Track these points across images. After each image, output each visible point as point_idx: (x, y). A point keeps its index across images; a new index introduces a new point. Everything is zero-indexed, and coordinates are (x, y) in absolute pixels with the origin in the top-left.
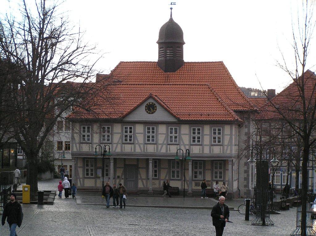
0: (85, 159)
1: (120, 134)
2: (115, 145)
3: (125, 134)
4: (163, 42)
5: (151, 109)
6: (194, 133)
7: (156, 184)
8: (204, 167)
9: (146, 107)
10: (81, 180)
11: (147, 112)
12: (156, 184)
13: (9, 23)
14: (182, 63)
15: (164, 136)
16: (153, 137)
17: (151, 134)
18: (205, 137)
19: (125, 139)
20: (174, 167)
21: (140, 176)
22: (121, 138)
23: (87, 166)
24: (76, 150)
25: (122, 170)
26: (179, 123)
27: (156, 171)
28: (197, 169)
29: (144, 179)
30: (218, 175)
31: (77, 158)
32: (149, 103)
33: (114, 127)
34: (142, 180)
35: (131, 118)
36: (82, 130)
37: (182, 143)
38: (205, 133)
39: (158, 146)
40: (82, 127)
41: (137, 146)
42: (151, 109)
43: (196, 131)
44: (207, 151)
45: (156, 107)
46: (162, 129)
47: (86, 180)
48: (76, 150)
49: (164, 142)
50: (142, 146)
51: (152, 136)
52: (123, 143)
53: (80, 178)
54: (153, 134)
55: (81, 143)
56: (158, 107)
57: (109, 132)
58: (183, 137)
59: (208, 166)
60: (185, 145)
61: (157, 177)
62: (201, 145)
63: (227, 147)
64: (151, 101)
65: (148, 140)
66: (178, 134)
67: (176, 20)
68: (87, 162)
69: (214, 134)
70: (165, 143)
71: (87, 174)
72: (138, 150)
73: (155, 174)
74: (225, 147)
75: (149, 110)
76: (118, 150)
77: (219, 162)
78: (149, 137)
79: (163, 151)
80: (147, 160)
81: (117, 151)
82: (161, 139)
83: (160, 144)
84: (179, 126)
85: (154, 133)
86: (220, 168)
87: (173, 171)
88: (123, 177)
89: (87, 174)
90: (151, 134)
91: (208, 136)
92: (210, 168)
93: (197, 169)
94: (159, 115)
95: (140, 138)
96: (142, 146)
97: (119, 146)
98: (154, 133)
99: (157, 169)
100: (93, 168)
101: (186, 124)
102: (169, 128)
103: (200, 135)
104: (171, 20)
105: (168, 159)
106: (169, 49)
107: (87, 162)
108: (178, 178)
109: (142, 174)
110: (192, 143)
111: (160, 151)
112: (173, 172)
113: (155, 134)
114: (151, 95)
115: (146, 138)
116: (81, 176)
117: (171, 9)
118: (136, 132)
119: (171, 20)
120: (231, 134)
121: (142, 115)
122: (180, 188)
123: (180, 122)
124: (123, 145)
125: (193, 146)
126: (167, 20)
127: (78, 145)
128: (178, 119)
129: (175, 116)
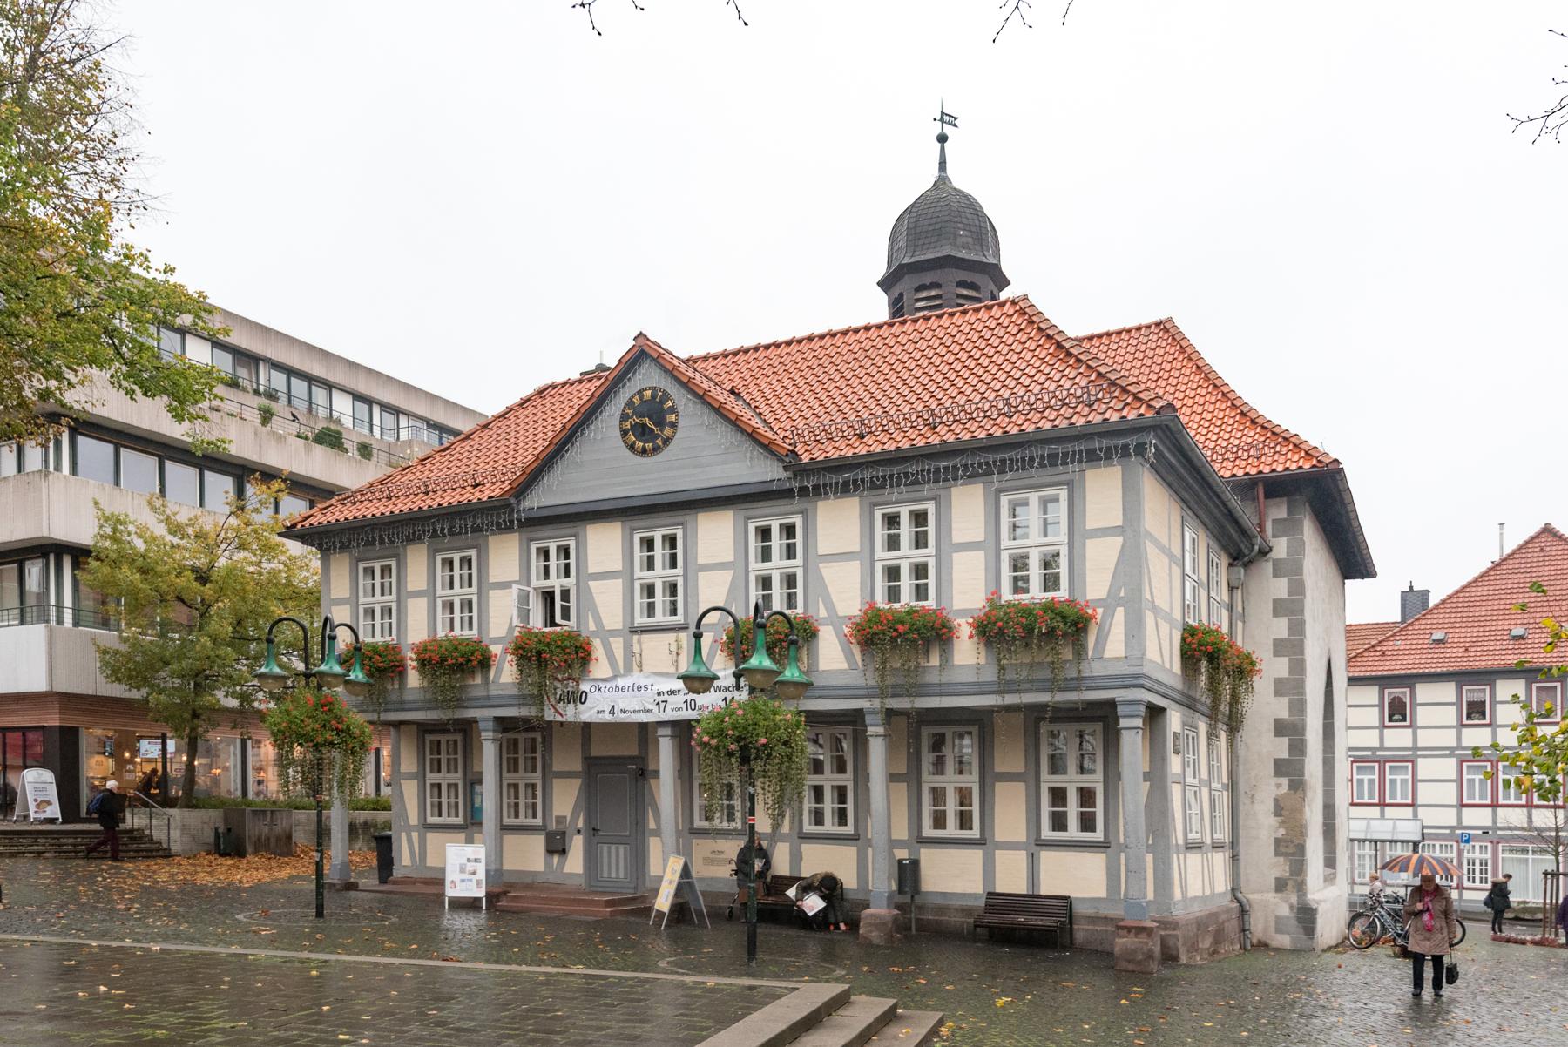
0: (926, 733)
1: (1120, 539)
3: (883, 556)
8: (546, 767)
10: (415, 835)
11: (632, 447)
15: (727, 576)
17: (906, 556)
18: (494, 594)
19: (1016, 579)
20: (1057, 766)
23: (1057, 766)
25: (575, 785)
26: (803, 492)
28: (822, 772)
32: (640, 393)
33: (333, 567)
36: (880, 533)
38: (957, 538)
42: (649, 428)
45: (673, 410)
53: (409, 829)
54: (891, 557)
55: (634, 631)
58: (828, 571)
59: (568, 759)
64: (647, 379)
66: (799, 561)
67: (960, 179)
68: (938, 743)
71: (1059, 823)
73: (1065, 805)
75: (642, 432)
84: (396, 556)
87: (933, 790)
88: (580, 825)
89: (1059, 823)
92: (1019, 766)
93: (822, 772)
100: (972, 780)
101: (845, 489)
102: (878, 514)
108: (966, 834)
112: (1059, 796)
113: (931, 549)
116: (413, 818)
118: (700, 561)
120: (1130, 527)
121: (605, 467)
125: (645, 637)
126: (924, 181)
128: (789, 459)
129: (768, 448)
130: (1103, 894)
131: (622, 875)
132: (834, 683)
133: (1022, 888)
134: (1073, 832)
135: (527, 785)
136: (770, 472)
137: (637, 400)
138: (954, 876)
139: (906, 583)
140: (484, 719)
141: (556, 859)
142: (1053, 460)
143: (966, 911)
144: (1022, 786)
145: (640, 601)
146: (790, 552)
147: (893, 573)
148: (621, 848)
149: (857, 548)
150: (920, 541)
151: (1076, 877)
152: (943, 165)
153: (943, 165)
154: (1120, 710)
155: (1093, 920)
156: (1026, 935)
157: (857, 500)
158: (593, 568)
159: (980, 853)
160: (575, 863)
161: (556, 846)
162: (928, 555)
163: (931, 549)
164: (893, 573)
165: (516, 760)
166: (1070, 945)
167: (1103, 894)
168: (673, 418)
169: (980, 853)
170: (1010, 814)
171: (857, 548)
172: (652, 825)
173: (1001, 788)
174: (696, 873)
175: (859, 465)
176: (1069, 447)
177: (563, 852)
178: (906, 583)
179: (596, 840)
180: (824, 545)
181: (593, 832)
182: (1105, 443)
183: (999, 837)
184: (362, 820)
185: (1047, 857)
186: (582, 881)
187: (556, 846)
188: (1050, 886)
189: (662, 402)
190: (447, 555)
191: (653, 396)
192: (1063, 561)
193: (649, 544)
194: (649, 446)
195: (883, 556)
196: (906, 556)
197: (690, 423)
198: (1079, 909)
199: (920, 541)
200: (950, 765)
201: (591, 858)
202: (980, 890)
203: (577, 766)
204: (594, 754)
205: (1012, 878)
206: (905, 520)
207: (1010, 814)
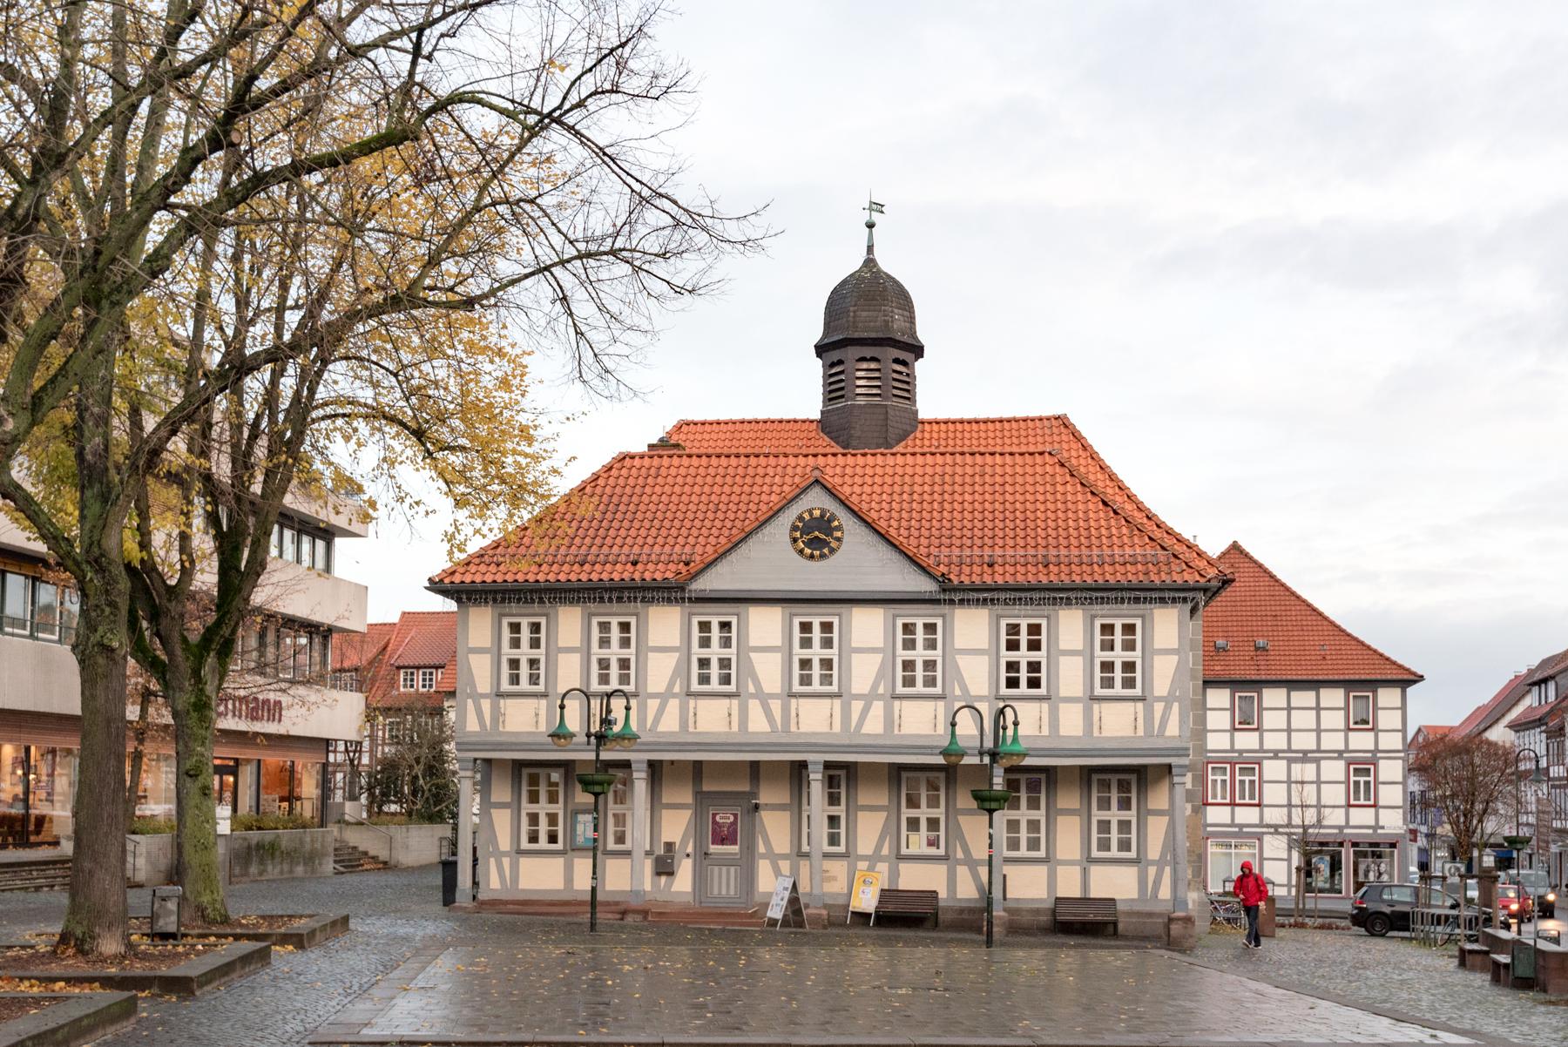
0: (525, 772)
2: (653, 705)
3: (698, 652)
4: (131, 294)
5: (816, 538)
6: (910, 645)
7: (834, 879)
9: (794, 528)
10: (506, 861)
12: (834, 879)
13: (595, 93)
14: (914, 422)
15: (878, 658)
16: (827, 664)
18: (1064, 661)
21: (767, 843)
22: (682, 670)
23: (913, 803)
24: (477, 729)
25: (687, 815)
27: (833, 820)
29: (784, 857)
30: (1114, 836)
31: (488, 761)
34: (774, 858)
35: (709, 583)
36: (596, 634)
37: (752, 689)
38: (1063, 646)
39: (1057, 709)
40: (505, 622)
41: (754, 707)
42: (816, 538)
43: (920, 636)
44: (1071, 723)
45: (839, 528)
46: (765, 627)
47: (524, 862)
48: (477, 729)
49: (875, 686)
50: (776, 706)
51: (1029, 664)
52: (689, 694)
53: (499, 855)
54: (806, 653)
56: (853, 535)
57: (1129, 646)
60: (764, 698)
61: (842, 849)
62: (1142, 699)
63: (1168, 708)
64: (816, 501)
65: (704, 679)
68: (534, 781)
69: (802, 647)
70: (881, 690)
71: (534, 838)
72: (758, 724)
74: (1159, 708)
75: (815, 543)
76: (669, 724)
77: (1114, 778)
78: (805, 664)
79: (874, 725)
80: (803, 765)
81: (661, 728)
82: (863, 673)
83: (1160, 699)
84: (546, 615)
85: (1133, 649)
86: (1125, 804)
88: (690, 849)
90: (715, 652)
91: (1079, 660)
94: (860, 562)
95: (769, 671)
96: (776, 706)
97: (673, 705)
98: (1133, 649)
99: (839, 811)
100: (558, 809)
102: (595, 621)
103: (1007, 656)
104: (870, 262)
105: (1082, 767)
106: (865, 365)
107: (534, 781)
108: (553, 846)
109: (775, 828)
110: (900, 689)
111: (657, 720)
112: (534, 819)
113: (543, 650)
114: (817, 473)
115: (1098, 674)
116: (505, 843)
117: (871, 226)
119: (870, 262)
121: (771, 560)
122: (943, 894)
123: (952, 593)
124: (692, 702)
125: (801, 701)
126: (853, 262)
127: (486, 705)
130: (1135, 896)
131: (732, 892)
132: (473, 739)
133: (1077, 894)
134: (1114, 852)
135: (1120, 822)
136: (925, 586)
137: (807, 517)
138: (1028, 886)
139: (614, 671)
140: (815, 763)
141: (663, 879)
142: (1137, 600)
143: (1037, 911)
144: (1077, 819)
145: (505, 671)
146: (726, 643)
147: (604, 664)
148: (732, 869)
149: (779, 643)
150: (625, 643)
151: (1116, 884)
152: (870, 249)
153: (870, 249)
154: (634, 766)
155: (1130, 914)
156: (1081, 924)
157: (678, 609)
158: (754, 641)
159: (945, 867)
160: (683, 881)
161: (664, 867)
162: (540, 653)
163: (543, 650)
164: (514, 664)
165: (1129, 799)
166: (1115, 934)
167: (1135, 896)
168: (838, 534)
169: (945, 867)
170: (1069, 837)
171: (779, 643)
172: (762, 849)
173: (666, 815)
174: (804, 888)
175: (653, 589)
176: (1148, 594)
177: (671, 874)
178: (614, 671)
179: (706, 862)
180: (654, 639)
181: (702, 856)
182: (1172, 594)
183: (1059, 856)
184: (254, 842)
185: (1095, 870)
186: (690, 899)
187: (664, 867)
188: (1096, 892)
189: (830, 521)
190: (515, 620)
191: (822, 516)
192: (542, 665)
193: (515, 628)
194: (817, 553)
195: (508, 652)
196: (615, 652)
197: (853, 535)
198: (1120, 907)
199: (1129, 646)
200: (543, 796)
201: (700, 878)
202: (1045, 896)
203: (688, 798)
204: (705, 789)
205: (1069, 887)
206: (816, 628)
207: (1069, 837)
